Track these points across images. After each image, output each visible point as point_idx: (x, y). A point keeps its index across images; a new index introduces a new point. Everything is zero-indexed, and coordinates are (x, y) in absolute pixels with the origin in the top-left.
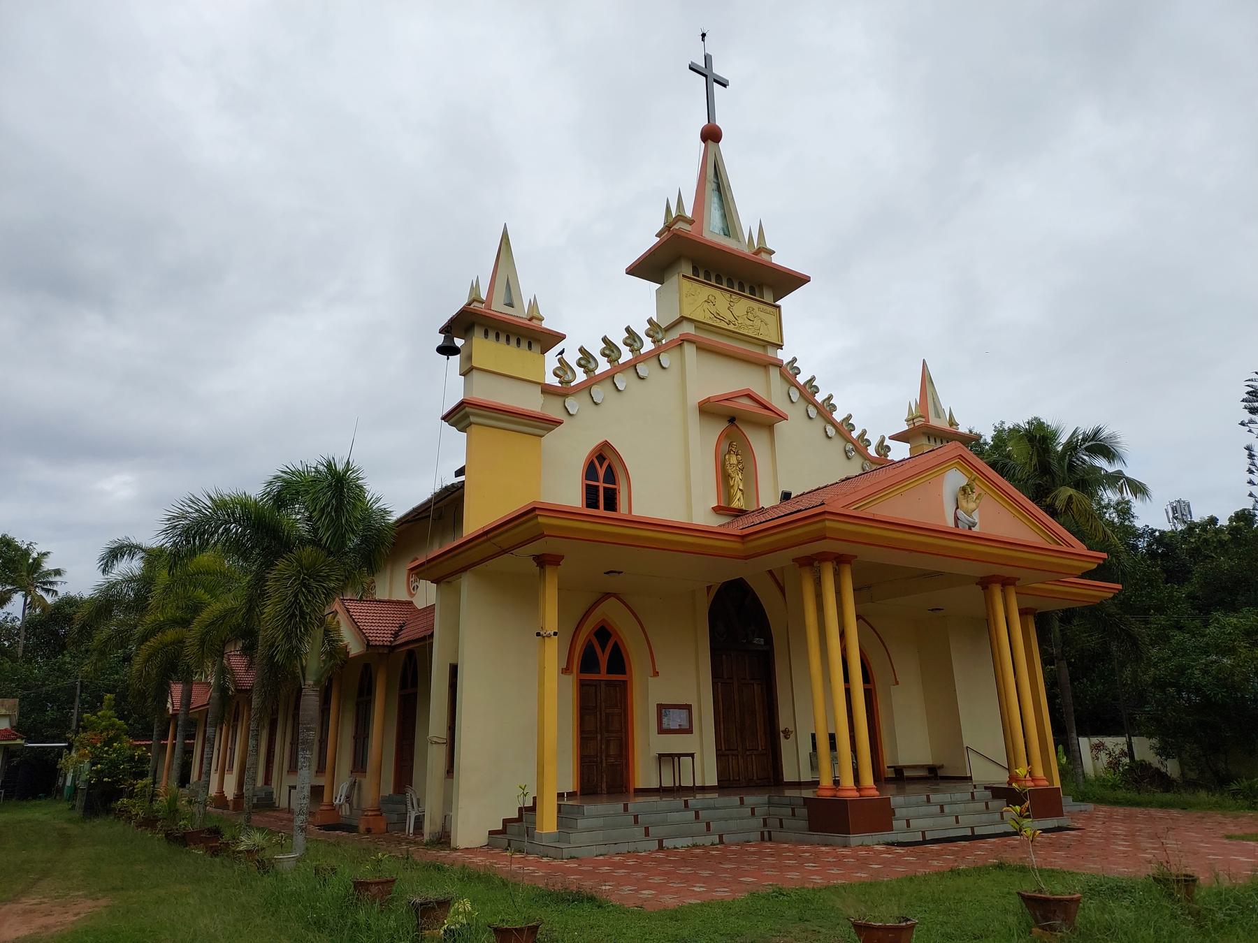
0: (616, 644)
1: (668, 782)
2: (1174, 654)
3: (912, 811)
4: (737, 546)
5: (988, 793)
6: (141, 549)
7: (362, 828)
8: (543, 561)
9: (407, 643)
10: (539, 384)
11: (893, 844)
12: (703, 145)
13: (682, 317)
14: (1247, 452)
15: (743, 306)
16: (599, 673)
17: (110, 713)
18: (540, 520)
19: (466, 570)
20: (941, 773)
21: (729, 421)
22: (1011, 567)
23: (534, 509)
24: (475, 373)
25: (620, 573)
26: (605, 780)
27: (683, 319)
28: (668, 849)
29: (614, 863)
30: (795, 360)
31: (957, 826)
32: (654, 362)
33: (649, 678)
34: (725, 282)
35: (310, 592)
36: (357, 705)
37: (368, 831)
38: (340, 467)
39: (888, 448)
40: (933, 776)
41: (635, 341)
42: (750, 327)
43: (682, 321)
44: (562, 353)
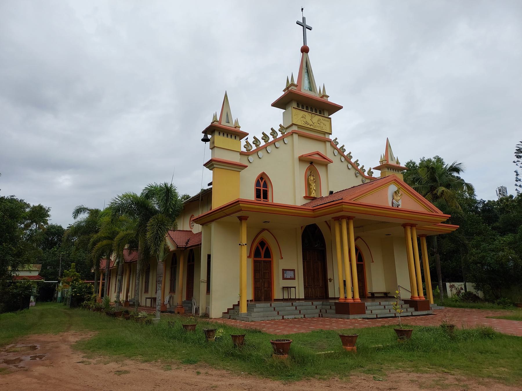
0: (267, 247)
1: (286, 297)
2: (482, 252)
3: (374, 308)
4: (311, 213)
5: (403, 302)
6: (88, 209)
7: (176, 312)
8: (241, 218)
9: (191, 246)
10: (239, 152)
11: (365, 318)
12: (302, 54)
13: (293, 124)
14: (516, 173)
15: (316, 118)
17: (74, 270)
18: (241, 205)
19: (213, 221)
20: (389, 295)
21: (310, 163)
22: (413, 221)
23: (238, 201)
24: (215, 148)
25: (269, 222)
26: (263, 295)
27: (293, 124)
28: (285, 319)
29: (267, 323)
30: (336, 139)
31: (390, 313)
32: (282, 142)
33: (279, 260)
34: (309, 109)
35: (161, 230)
36: (171, 268)
37: (178, 313)
38: (169, 185)
39: (372, 172)
40: (386, 296)
41: (275, 134)
42: (319, 127)
43: (293, 125)
44: (247, 139)
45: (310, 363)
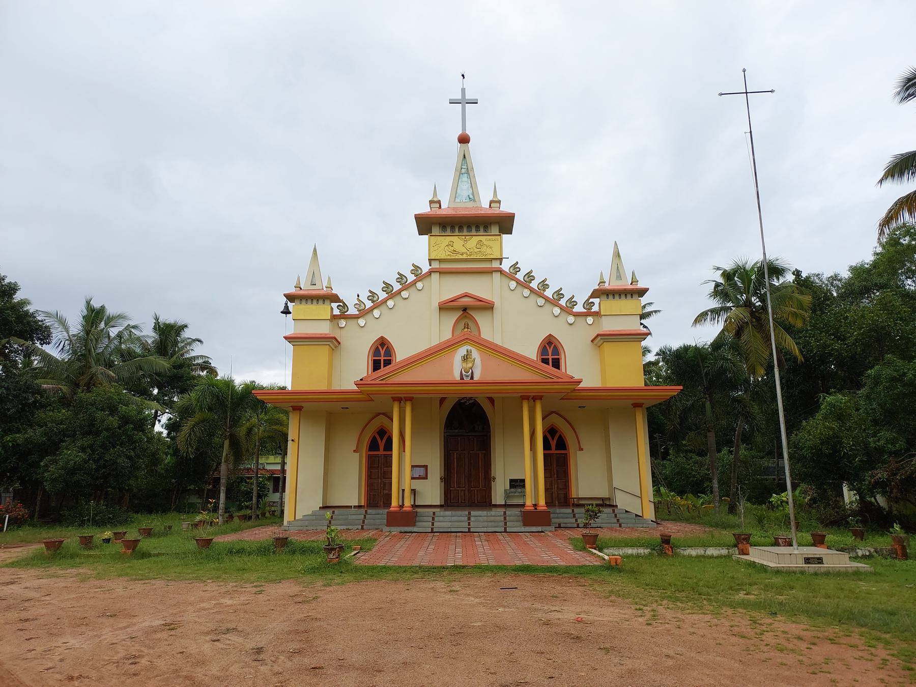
0: (560, 436)
16: (551, 450)
21: (463, 311)
45: (705, 601)
